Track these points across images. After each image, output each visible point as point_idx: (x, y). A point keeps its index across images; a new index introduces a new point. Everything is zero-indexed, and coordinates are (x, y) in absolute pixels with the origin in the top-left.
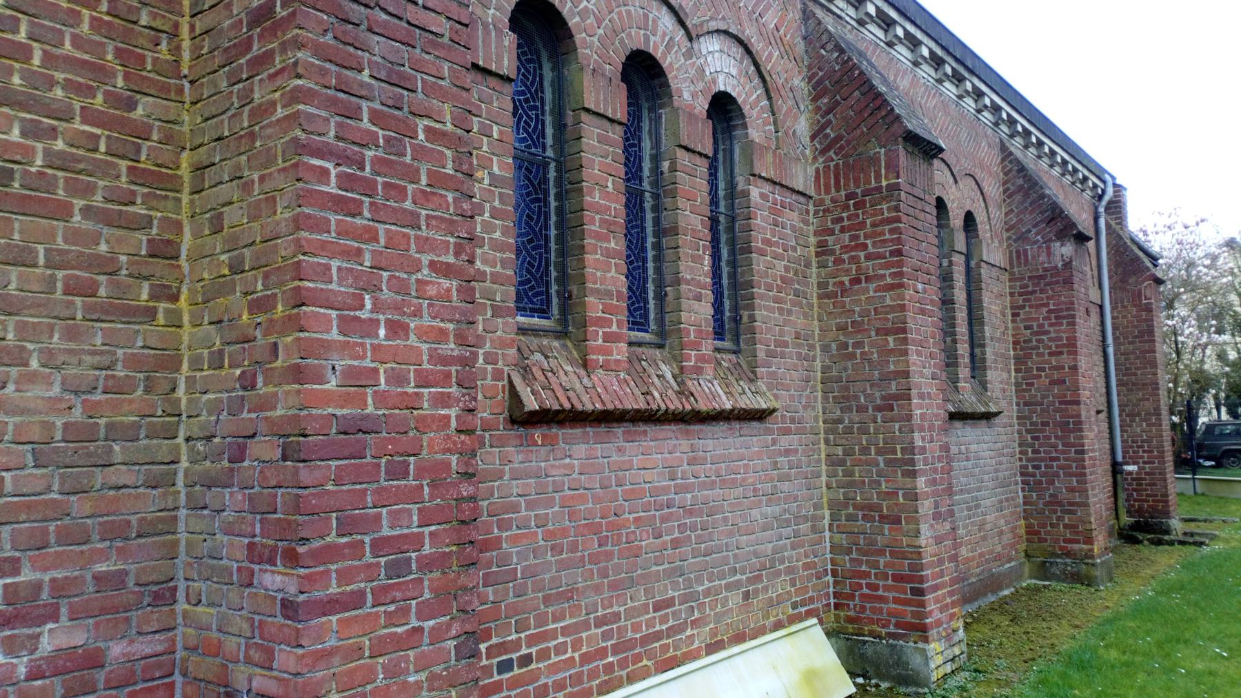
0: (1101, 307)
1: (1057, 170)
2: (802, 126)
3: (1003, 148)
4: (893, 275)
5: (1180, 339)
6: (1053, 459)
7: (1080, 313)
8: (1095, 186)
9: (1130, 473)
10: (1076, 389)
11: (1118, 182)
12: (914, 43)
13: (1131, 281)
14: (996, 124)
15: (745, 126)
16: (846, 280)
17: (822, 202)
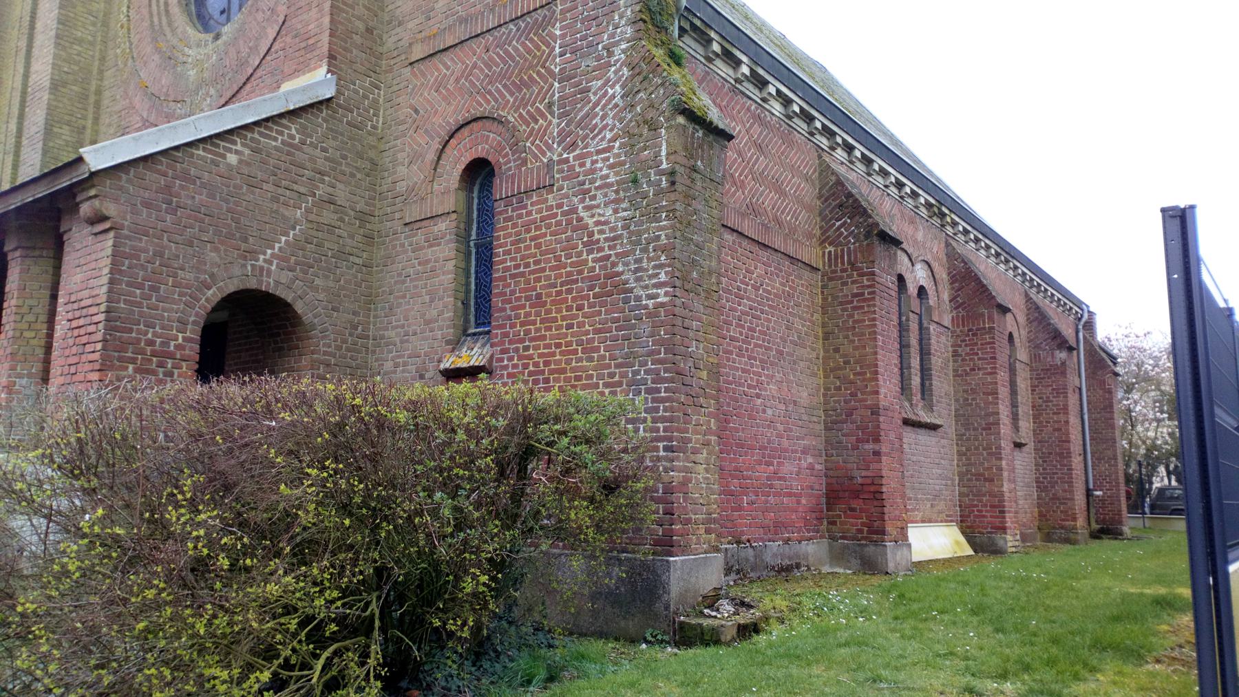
0: (1080, 389)
1: (1054, 305)
2: (946, 296)
3: (1027, 295)
4: (992, 368)
5: (1133, 414)
6: (1054, 474)
7: (1070, 391)
8: (1077, 312)
9: (1098, 496)
10: (1068, 434)
11: (1091, 310)
12: (988, 247)
13: (1100, 373)
14: (1023, 282)
15: (928, 299)
16: (968, 369)
17: (955, 331)
